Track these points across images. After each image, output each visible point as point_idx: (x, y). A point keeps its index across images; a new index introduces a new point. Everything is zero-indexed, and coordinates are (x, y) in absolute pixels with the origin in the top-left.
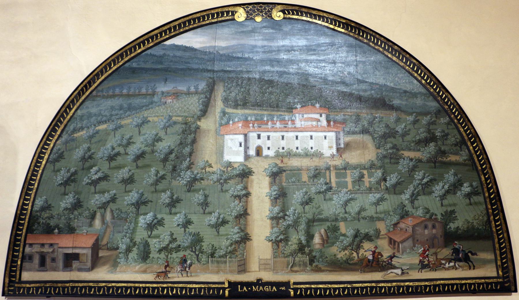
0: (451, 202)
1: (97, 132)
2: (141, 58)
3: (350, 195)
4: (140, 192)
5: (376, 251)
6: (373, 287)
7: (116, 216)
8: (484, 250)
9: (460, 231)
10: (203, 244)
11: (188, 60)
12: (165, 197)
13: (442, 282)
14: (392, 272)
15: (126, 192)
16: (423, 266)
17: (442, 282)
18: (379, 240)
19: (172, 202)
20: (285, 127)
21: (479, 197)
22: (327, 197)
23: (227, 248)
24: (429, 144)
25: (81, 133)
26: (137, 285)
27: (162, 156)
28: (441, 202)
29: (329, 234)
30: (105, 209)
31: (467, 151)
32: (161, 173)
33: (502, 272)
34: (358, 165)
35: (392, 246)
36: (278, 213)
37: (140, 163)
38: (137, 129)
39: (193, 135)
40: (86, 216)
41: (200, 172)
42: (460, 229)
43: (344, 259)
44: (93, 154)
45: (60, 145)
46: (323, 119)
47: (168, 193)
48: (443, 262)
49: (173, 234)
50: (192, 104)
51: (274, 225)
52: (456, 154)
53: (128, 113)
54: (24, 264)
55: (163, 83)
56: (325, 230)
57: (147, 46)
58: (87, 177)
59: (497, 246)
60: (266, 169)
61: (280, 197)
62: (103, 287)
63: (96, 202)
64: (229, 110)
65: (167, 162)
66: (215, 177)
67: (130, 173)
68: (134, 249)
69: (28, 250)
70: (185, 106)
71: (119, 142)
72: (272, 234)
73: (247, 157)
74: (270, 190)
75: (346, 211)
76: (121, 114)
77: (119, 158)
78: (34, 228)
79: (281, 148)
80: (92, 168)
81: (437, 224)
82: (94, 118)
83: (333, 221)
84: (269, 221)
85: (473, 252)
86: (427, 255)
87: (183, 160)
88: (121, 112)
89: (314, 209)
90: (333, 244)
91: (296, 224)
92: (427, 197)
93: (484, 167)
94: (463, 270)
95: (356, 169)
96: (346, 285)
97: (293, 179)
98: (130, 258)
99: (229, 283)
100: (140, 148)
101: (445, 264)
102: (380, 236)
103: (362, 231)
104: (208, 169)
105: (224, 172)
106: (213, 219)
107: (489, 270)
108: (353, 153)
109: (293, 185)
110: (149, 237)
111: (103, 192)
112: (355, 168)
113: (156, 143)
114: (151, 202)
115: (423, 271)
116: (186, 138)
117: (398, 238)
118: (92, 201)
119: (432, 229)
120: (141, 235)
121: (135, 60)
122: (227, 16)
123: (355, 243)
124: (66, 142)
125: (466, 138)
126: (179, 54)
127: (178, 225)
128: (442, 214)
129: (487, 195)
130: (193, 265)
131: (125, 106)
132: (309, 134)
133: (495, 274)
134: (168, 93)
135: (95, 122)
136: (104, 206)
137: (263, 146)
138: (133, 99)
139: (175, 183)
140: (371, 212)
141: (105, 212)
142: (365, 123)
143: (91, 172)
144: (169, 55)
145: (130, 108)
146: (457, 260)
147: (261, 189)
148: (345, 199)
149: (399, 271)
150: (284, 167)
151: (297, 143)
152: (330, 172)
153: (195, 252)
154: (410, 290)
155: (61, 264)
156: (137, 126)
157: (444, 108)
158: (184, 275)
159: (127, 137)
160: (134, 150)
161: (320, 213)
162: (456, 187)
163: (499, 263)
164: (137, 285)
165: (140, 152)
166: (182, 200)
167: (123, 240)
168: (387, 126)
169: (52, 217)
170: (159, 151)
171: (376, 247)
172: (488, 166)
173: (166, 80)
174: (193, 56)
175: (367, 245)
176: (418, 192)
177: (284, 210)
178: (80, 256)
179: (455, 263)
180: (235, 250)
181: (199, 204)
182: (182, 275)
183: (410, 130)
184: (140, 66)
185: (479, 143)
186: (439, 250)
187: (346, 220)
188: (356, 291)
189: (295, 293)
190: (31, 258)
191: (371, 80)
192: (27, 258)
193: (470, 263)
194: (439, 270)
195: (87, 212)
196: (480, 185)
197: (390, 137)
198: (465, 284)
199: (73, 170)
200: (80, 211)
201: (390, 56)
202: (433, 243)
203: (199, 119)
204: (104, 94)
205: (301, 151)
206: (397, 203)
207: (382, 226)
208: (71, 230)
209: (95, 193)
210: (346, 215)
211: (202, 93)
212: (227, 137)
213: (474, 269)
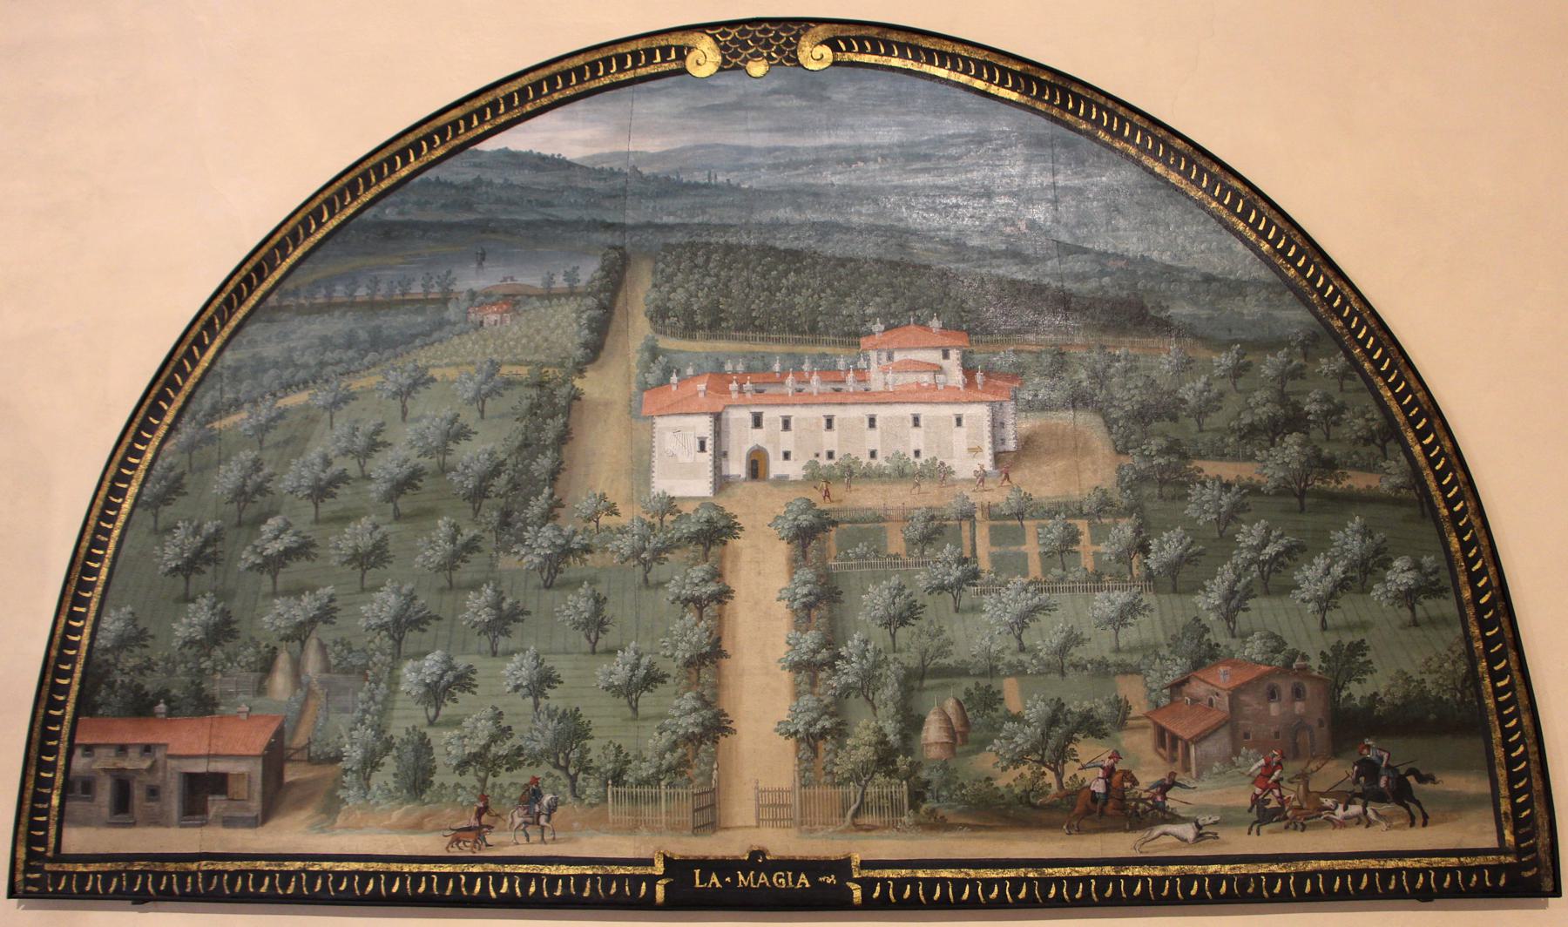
1: (281, 415)
3: (1034, 595)
4: (404, 591)
5: (1117, 768)
6: (1108, 878)
7: (334, 662)
8: (1456, 766)
9: (1380, 709)
10: (589, 743)
12: (477, 605)
14: (1165, 834)
16: (1264, 815)
19: (499, 618)
20: (837, 390)
21: (1442, 602)
22: (965, 601)
24: (1282, 439)
26: (394, 867)
27: (470, 484)
28: (1319, 617)
29: (969, 714)
30: (303, 643)
31: (1402, 458)
32: (468, 532)
33: (1514, 833)
35: (1165, 753)
36: (815, 652)
37: (404, 504)
38: (396, 404)
39: (560, 420)
40: (248, 664)
41: (580, 530)
43: (1017, 791)
44: (269, 478)
45: (172, 453)
47: (488, 591)
48: (1328, 802)
52: (1368, 468)
54: (70, 805)
55: (474, 265)
56: (959, 703)
57: (427, 157)
58: (249, 548)
59: (1499, 753)
60: (778, 517)
61: (822, 600)
62: (297, 873)
64: (667, 343)
65: (486, 502)
66: (626, 544)
67: (377, 536)
68: (387, 759)
69: (80, 763)
71: (343, 444)
72: (795, 713)
73: (722, 482)
74: (792, 579)
75: (1021, 643)
76: (352, 360)
79: (824, 455)
80: (264, 522)
81: (1307, 686)
82: (272, 372)
83: (983, 675)
84: (786, 676)
85: (1423, 772)
86: (1277, 782)
88: (351, 353)
89: (925, 639)
90: (982, 745)
91: (868, 683)
92: (1276, 602)
93: (1457, 509)
94: (1390, 827)
96: (1021, 872)
97: (861, 548)
98: (374, 788)
99: (668, 861)
101: (1332, 810)
104: (604, 520)
105: (652, 527)
106: (619, 669)
107: (1474, 828)
108: (1045, 468)
109: (859, 566)
110: (431, 723)
111: (296, 592)
113: (452, 445)
114: (438, 619)
115: (1264, 829)
116: (539, 429)
118: (265, 619)
119: (1293, 701)
120: (407, 718)
121: (392, 198)
122: (664, 60)
123: (1052, 743)
124: (191, 447)
125: (1400, 418)
127: (517, 688)
128: (1322, 653)
129: (1467, 594)
131: (363, 335)
132: (910, 410)
133: (1491, 841)
134: (488, 295)
135: (276, 385)
136: (300, 633)
139: (506, 562)
140: (1099, 646)
143: (261, 534)
144: (490, 184)
145: (378, 342)
146: (1372, 795)
147: (763, 579)
148: (1020, 607)
149: (1188, 831)
150: (833, 510)
151: (873, 439)
152: (973, 527)
153: (565, 769)
154: (1223, 890)
157: (1329, 327)
159: (369, 427)
160: (386, 466)
161: (942, 651)
162: (1368, 569)
163: (1505, 806)
164: (394, 867)
165: (406, 470)
166: (529, 613)
169: (149, 666)
170: (460, 467)
171: (1116, 756)
172: (1471, 505)
173: (482, 258)
175: (1088, 750)
177: (832, 641)
178: (230, 781)
179: (1365, 806)
180: (685, 763)
181: (577, 625)
182: (527, 836)
185: (1441, 434)
186: (1313, 766)
187: (1024, 673)
188: (1053, 891)
189: (867, 894)
190: (88, 786)
192: (79, 786)
193: (1413, 807)
196: (1445, 564)
198: (1397, 871)
199: (209, 527)
200: (230, 647)
202: (1296, 745)
204: (303, 301)
205: (885, 464)
206: (1181, 620)
207: (1133, 691)
209: (275, 594)
212: (660, 423)
213: (1425, 824)
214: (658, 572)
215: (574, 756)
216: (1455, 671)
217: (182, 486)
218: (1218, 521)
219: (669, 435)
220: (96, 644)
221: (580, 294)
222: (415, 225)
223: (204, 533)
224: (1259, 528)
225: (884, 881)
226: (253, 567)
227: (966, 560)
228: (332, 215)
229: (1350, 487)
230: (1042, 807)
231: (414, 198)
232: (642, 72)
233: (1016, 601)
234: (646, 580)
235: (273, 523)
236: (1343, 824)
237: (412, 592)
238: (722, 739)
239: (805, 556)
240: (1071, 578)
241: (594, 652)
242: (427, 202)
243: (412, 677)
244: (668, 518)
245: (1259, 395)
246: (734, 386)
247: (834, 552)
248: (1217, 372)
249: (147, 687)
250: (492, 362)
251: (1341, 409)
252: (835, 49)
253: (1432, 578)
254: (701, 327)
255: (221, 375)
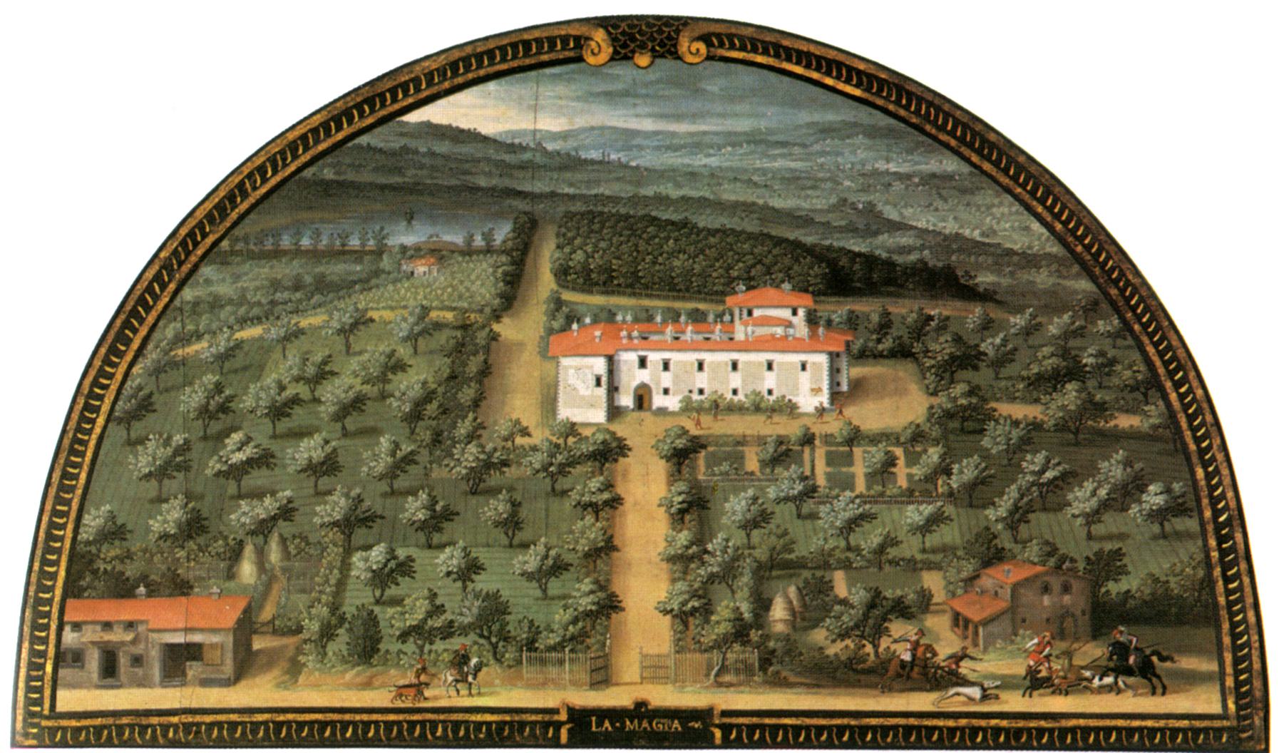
0: (1114, 530)
1: (239, 345)
2: (344, 157)
3: (859, 506)
4: (353, 494)
5: (922, 642)
7: (294, 552)
9: (1131, 603)
10: (508, 618)
11: (467, 166)
12: (415, 508)
13: (1082, 722)
14: (958, 694)
15: (318, 494)
16: (1035, 682)
17: (1082, 722)
18: (929, 616)
19: (432, 517)
20: (708, 339)
21: (1186, 519)
23: (566, 630)
24: (1063, 386)
25: (196, 347)
26: (347, 717)
27: (407, 408)
30: (266, 537)
31: (1161, 403)
32: (407, 448)
33: (1236, 703)
34: (522, 270)
35: (959, 631)
36: (687, 548)
37: (351, 423)
38: (340, 340)
39: (481, 357)
40: (217, 554)
41: (500, 447)
42: (1133, 597)
43: (843, 658)
44: (230, 399)
45: (139, 375)
46: (800, 319)
47: (423, 496)
48: (1088, 674)
49: (435, 594)
50: (478, 277)
51: (677, 575)
53: (317, 298)
54: (62, 672)
55: (405, 223)
56: (798, 589)
57: (359, 124)
58: (216, 458)
59: (1227, 640)
60: (659, 441)
61: (694, 508)
62: (265, 723)
63: (243, 519)
64: (567, 296)
65: (421, 423)
66: (537, 460)
67: (328, 449)
68: (341, 631)
69: (69, 637)
70: (462, 282)
71: (295, 372)
73: (614, 412)
75: (848, 543)
76: (300, 301)
77: (298, 411)
78: (82, 583)
79: (696, 391)
80: (228, 436)
82: (228, 308)
84: (664, 565)
85: (1165, 654)
87: (458, 416)
88: (298, 295)
89: (773, 538)
91: (728, 573)
92: (1051, 515)
93: (1204, 445)
94: (1135, 696)
95: (876, 445)
96: (845, 721)
97: (725, 467)
98: (330, 654)
99: (571, 711)
100: (351, 388)
101: (1090, 680)
102: (932, 608)
103: (888, 593)
104: (519, 440)
105: (557, 446)
106: (531, 560)
107: (1204, 697)
110: (378, 602)
111: (258, 495)
112: (874, 439)
113: (390, 376)
114: (382, 517)
115: (1035, 693)
116: (465, 365)
117: (975, 614)
118: (233, 517)
120: (358, 597)
121: (329, 160)
122: (563, 49)
124: (158, 371)
125: (1161, 371)
126: (443, 147)
127: (449, 574)
129: (1208, 514)
130: (485, 669)
131: (308, 279)
132: (764, 357)
133: (1216, 708)
134: (418, 249)
135: (232, 320)
136: (263, 529)
137: (653, 386)
138: (327, 263)
139: (437, 473)
140: (910, 547)
141: (266, 542)
142: (904, 332)
143: (225, 446)
144: (416, 152)
145: (323, 286)
147: (646, 487)
148: (847, 515)
149: (975, 692)
151: (736, 380)
152: (813, 450)
153: (488, 638)
155: (156, 672)
156: (341, 331)
157: (1106, 294)
158: (462, 692)
159: (318, 358)
160: (333, 393)
161: (788, 548)
162: (1129, 491)
163: (1230, 682)
164: (347, 717)
165: (351, 394)
166: (458, 514)
167: (313, 611)
168: (958, 339)
169: (129, 556)
170: (397, 394)
171: (921, 633)
173: (410, 217)
174: (480, 155)
175: (898, 628)
176: (1027, 504)
177: (700, 540)
178: (205, 648)
179: (1116, 678)
180: (584, 634)
181: (497, 524)
182: (458, 691)
183: (1015, 349)
184: (342, 178)
186: (1076, 646)
190: (77, 658)
191: (921, 224)
192: (69, 657)
193: (1154, 680)
194: (1074, 692)
195: (221, 542)
197: (962, 367)
199: (178, 439)
200: (201, 540)
201: (975, 158)
203: (498, 318)
204: (252, 247)
205: (743, 399)
208: (181, 588)
209: (240, 496)
210: (851, 555)
211: (503, 252)
212: (565, 362)
213: (1163, 694)
214: (563, 483)
215: (495, 628)
216: (1194, 575)
217: (151, 404)
218: (1007, 451)
219: (572, 371)
220: (79, 538)
221: (496, 251)
222: (353, 185)
223: (174, 444)
224: (1040, 458)
225: (739, 726)
226: (219, 474)
227: (807, 478)
228: (275, 172)
229: (1116, 426)
230: (864, 672)
231: (348, 160)
232: (545, 58)
233: (845, 510)
234: (553, 489)
235: (236, 437)
236: (1103, 689)
237: (359, 496)
238: (614, 615)
239: (679, 472)
240: (888, 493)
241: (511, 546)
242: (360, 166)
243: (361, 565)
244: (571, 440)
245: (1046, 350)
246: (624, 333)
247: (703, 469)
248: (1013, 331)
249: (128, 574)
250: (423, 306)
251: (1113, 362)
252: (709, 44)
253: (1180, 501)
254: (597, 284)
255: (181, 310)
